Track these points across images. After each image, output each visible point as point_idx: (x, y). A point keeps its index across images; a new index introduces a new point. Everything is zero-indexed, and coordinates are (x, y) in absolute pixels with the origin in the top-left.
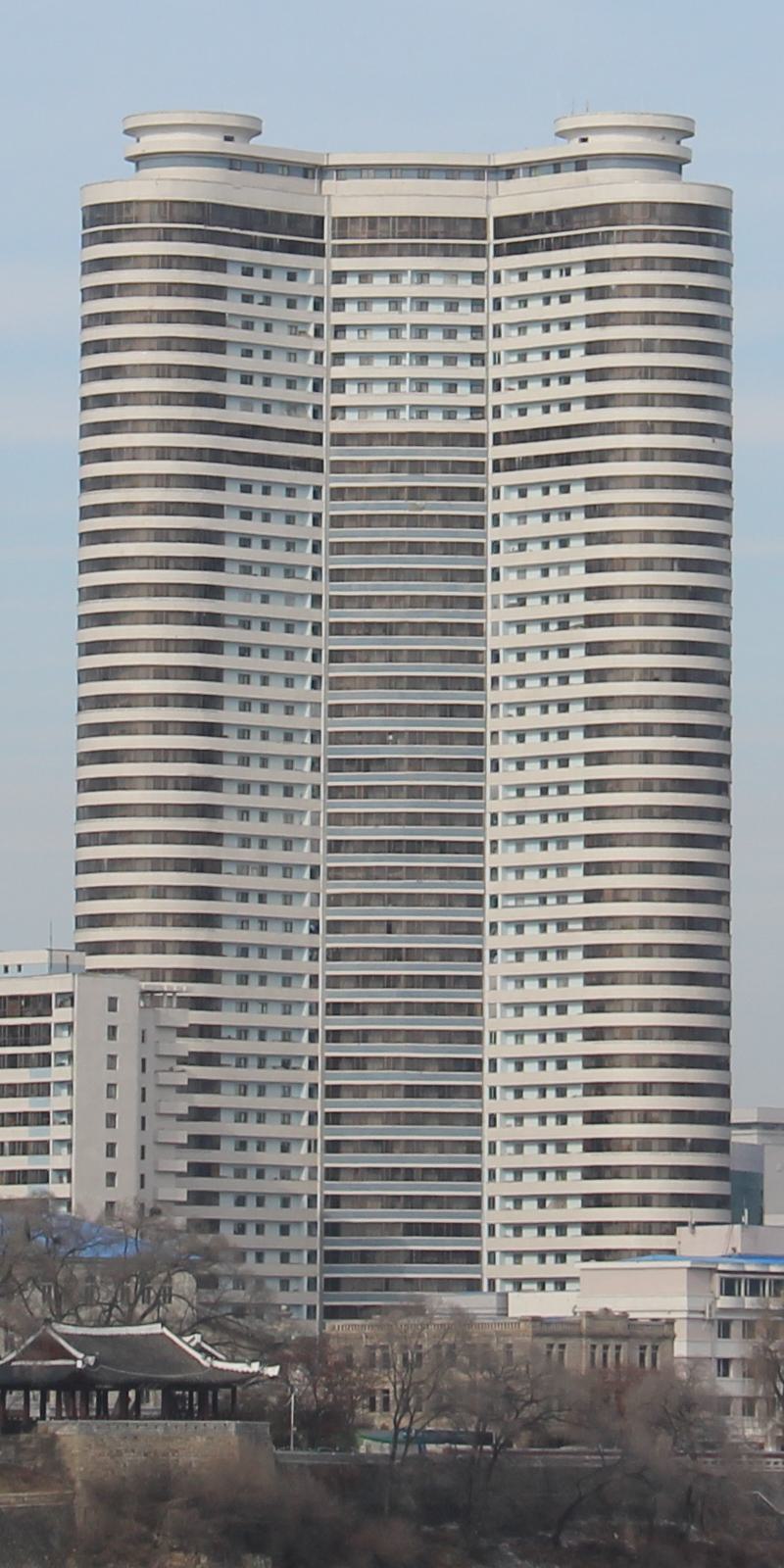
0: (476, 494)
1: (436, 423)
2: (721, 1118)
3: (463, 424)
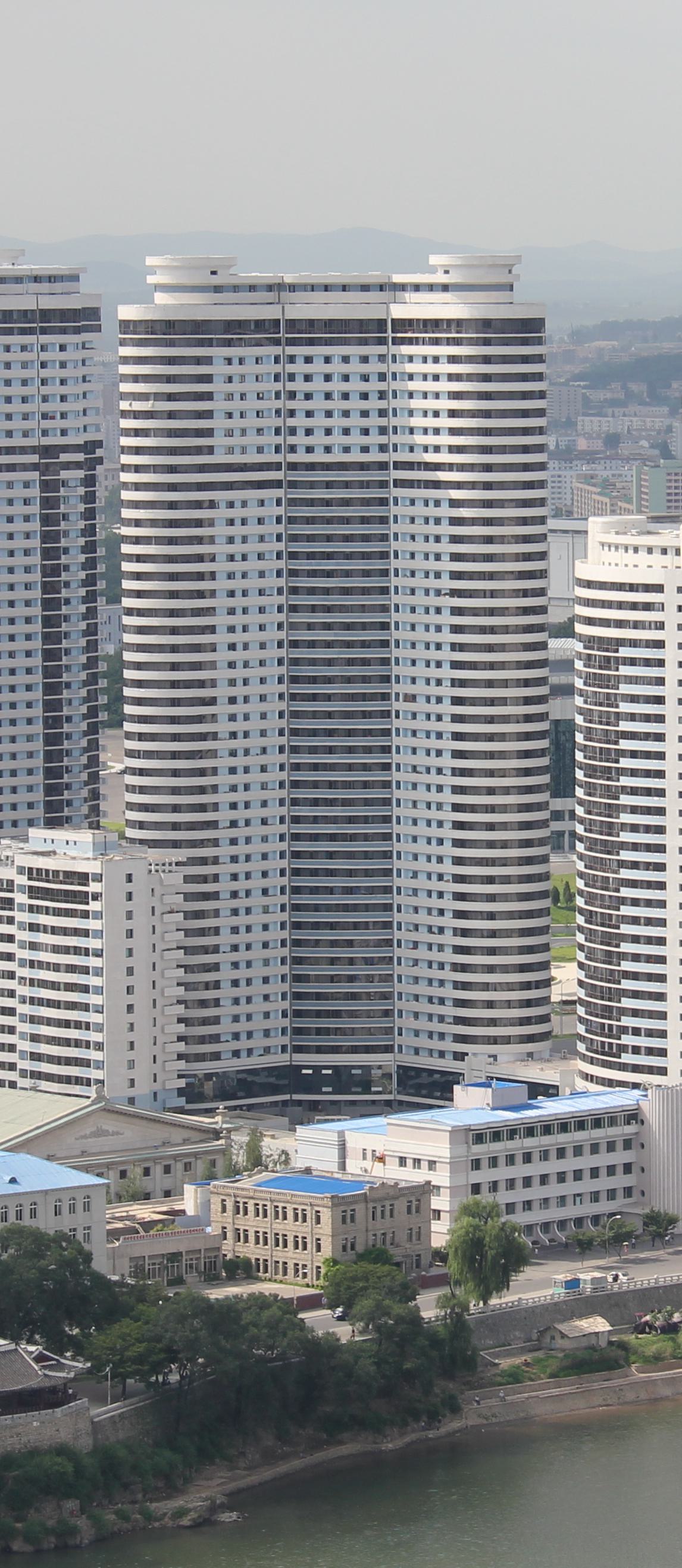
0: (383, 502)
1: (356, 456)
2: (545, 1001)
3: (375, 456)
